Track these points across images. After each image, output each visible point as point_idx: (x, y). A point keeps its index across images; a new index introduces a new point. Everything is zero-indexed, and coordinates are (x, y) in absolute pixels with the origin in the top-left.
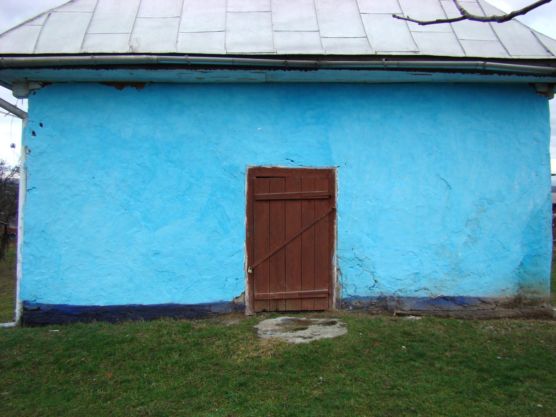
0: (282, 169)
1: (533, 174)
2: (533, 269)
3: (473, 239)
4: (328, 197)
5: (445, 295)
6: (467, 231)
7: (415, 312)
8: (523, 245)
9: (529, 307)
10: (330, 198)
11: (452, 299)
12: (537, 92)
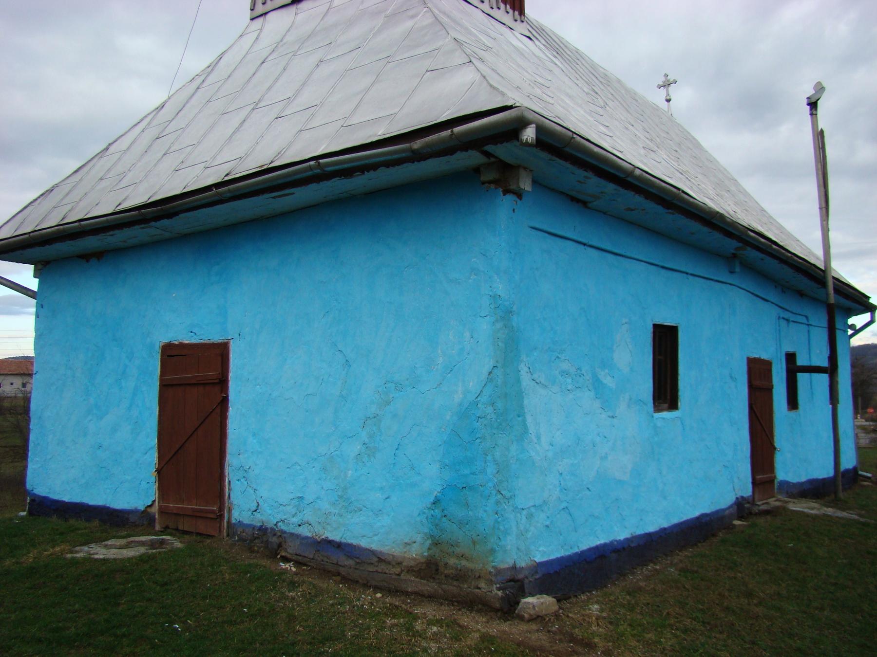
0: (187, 344)
1: (467, 334)
2: (459, 513)
3: (370, 450)
4: (217, 381)
5: (330, 538)
6: (364, 435)
7: (300, 558)
8: (444, 466)
9: (455, 583)
10: (223, 382)
11: (339, 546)
12: (483, 183)
